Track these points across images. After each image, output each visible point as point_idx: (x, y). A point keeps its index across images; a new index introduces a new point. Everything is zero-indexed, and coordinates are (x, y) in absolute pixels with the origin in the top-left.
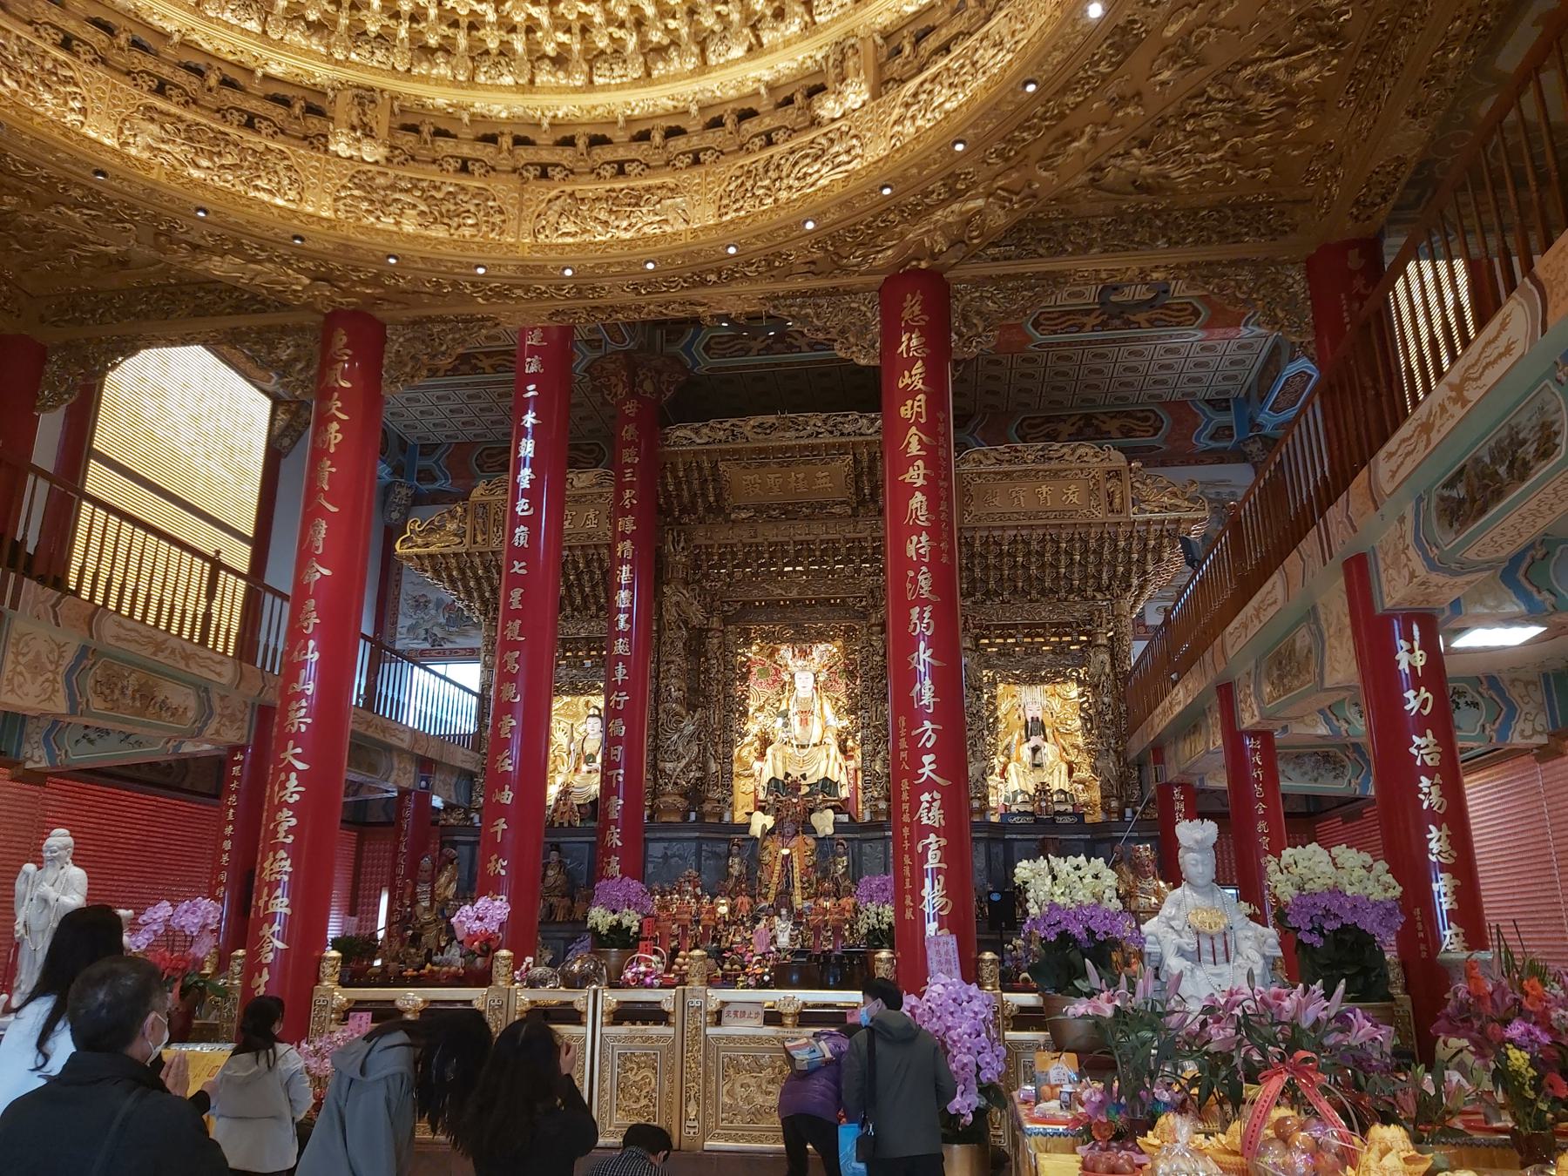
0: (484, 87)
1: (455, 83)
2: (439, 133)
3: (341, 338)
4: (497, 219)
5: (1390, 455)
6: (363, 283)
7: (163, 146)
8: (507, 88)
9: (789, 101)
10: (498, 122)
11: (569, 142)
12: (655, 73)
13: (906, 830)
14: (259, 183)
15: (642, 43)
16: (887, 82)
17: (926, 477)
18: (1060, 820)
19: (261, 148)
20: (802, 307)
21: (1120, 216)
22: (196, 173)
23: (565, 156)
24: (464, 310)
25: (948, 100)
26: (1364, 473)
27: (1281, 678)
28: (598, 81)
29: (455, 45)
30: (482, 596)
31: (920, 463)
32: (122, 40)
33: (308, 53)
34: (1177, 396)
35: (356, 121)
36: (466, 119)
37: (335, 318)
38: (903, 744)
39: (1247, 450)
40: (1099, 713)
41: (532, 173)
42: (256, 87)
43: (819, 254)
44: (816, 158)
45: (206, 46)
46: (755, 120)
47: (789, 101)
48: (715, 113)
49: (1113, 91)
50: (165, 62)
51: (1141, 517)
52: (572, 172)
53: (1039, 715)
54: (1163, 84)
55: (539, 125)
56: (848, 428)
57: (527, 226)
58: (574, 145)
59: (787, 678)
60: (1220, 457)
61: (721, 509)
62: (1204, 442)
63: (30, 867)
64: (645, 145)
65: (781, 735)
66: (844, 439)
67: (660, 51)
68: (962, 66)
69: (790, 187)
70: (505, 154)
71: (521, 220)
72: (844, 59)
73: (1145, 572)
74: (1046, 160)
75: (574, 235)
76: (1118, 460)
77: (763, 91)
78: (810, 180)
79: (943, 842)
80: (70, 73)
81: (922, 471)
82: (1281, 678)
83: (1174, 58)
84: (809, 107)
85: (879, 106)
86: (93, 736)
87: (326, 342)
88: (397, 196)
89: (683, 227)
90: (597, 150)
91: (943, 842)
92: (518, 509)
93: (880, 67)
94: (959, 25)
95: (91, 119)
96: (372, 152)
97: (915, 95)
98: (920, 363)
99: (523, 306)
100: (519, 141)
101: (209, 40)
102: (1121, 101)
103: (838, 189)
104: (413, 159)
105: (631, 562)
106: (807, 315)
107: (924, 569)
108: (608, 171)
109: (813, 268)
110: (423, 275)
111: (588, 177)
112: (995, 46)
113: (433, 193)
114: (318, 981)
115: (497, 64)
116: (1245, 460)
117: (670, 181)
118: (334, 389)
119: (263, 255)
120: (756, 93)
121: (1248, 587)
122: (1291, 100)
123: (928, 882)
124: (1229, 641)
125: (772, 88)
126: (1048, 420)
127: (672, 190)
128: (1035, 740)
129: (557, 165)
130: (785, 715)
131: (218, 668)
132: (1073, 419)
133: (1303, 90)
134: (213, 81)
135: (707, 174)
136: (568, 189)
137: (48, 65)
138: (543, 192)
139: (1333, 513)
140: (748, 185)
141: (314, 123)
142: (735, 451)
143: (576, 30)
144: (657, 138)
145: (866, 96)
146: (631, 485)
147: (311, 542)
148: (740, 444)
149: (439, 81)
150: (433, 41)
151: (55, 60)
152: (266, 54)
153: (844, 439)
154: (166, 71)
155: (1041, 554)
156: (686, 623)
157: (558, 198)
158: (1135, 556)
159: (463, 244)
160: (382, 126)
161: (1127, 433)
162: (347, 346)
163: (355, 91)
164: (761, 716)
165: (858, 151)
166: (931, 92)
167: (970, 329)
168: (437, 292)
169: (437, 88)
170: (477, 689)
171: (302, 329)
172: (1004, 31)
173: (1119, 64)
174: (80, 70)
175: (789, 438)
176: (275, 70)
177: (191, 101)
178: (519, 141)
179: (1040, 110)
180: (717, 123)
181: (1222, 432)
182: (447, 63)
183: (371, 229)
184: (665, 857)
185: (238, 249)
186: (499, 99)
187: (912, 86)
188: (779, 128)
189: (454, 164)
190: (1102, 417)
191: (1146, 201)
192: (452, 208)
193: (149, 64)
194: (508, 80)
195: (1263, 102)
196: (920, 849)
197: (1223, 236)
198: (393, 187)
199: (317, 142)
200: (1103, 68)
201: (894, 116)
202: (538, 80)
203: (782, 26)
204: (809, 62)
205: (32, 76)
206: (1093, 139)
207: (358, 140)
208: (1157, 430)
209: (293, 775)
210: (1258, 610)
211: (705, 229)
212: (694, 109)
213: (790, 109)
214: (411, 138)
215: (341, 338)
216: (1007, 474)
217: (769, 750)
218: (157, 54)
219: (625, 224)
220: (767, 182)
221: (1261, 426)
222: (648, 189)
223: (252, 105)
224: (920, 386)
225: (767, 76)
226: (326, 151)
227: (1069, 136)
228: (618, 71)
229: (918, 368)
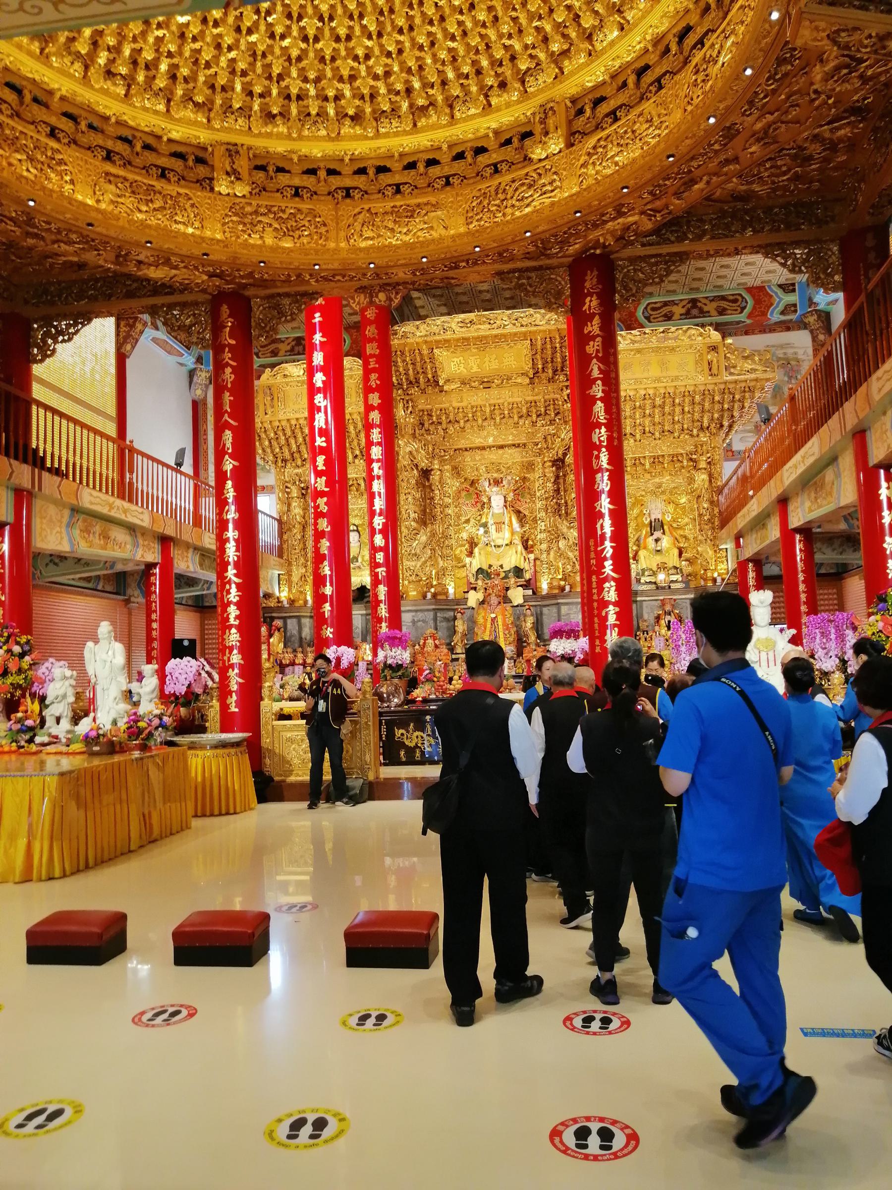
0: (308, 138)
1: (289, 137)
2: (280, 170)
3: (225, 310)
4: (323, 230)
5: (879, 379)
6: (242, 277)
7: (119, 200)
8: (322, 138)
9: (508, 142)
10: (316, 160)
11: (362, 171)
12: (419, 124)
13: (595, 604)
14: (177, 218)
15: (411, 106)
16: (575, 133)
17: (603, 391)
18: (673, 586)
19: (174, 194)
20: (519, 278)
21: (723, 214)
22: (141, 216)
23: (360, 181)
24: (302, 289)
25: (617, 155)
26: (865, 385)
27: (816, 498)
28: (382, 130)
29: (289, 113)
30: (272, 452)
31: (599, 382)
32: (83, 126)
33: (195, 123)
34: (758, 283)
35: (229, 169)
36: (296, 160)
37: (218, 299)
38: (592, 555)
39: (806, 321)
40: (700, 515)
41: (340, 194)
42: (164, 148)
43: (534, 249)
44: (530, 186)
45: (131, 123)
46: (486, 155)
47: (508, 142)
48: (459, 149)
49: (722, 157)
50: (108, 137)
51: (730, 378)
52: (366, 193)
53: (660, 517)
54: (751, 153)
55: (342, 160)
56: (525, 321)
57: (342, 234)
58: (367, 174)
59: (485, 500)
60: (787, 327)
61: (437, 383)
62: (775, 316)
63: (90, 644)
64: (413, 172)
65: (484, 539)
66: (523, 329)
67: (423, 109)
68: (626, 132)
69: (513, 206)
70: (322, 183)
71: (338, 229)
72: (546, 117)
73: (732, 416)
74: (678, 194)
75: (372, 239)
76: (716, 336)
77: (491, 135)
78: (526, 202)
79: (617, 609)
80: (61, 157)
81: (601, 388)
82: (816, 498)
83: (758, 140)
84: (522, 148)
85: (571, 153)
86: (57, 561)
87: (215, 315)
88: (260, 218)
89: (443, 232)
90: (382, 176)
91: (617, 609)
92: (316, 401)
93: (570, 122)
94: (622, 98)
95: (78, 187)
96: (241, 190)
97: (594, 148)
98: (597, 317)
99: (339, 284)
100: (331, 172)
101: (134, 118)
102: (727, 162)
103: (547, 212)
104: (265, 190)
105: (379, 426)
106: (523, 284)
107: (604, 450)
108: (389, 192)
109: (528, 256)
110: (280, 272)
111: (376, 196)
112: (647, 121)
113: (281, 214)
114: (262, 699)
115: (315, 122)
116: (805, 328)
117: (433, 200)
118: (225, 346)
119: (182, 265)
120: (487, 136)
121: (800, 441)
122: (833, 147)
123: (608, 632)
124: (786, 475)
125: (497, 133)
126: (666, 304)
127: (433, 205)
128: (657, 534)
129: (356, 188)
130: (485, 525)
131: (141, 517)
132: (684, 303)
133: (840, 140)
134: (138, 148)
135: (457, 195)
136: (367, 207)
137: (49, 154)
138: (348, 208)
139: (847, 405)
140: (485, 203)
141: (202, 171)
142: (446, 341)
143: (367, 98)
144: (421, 167)
145: (562, 146)
146: (374, 370)
147: (224, 445)
148: (449, 335)
149: (279, 136)
150: (275, 111)
151: (52, 149)
152: (169, 126)
153: (523, 329)
154: (110, 144)
155: (662, 406)
156: (417, 466)
157: (360, 213)
158: (726, 406)
159: (303, 250)
160: (244, 170)
161: (722, 312)
162: (229, 316)
163: (225, 147)
164: (468, 527)
165: (558, 183)
166: (605, 147)
167: (627, 291)
168: (287, 281)
169: (276, 141)
170: (276, 515)
171: (196, 304)
172: (654, 113)
173: (725, 145)
174: (70, 154)
175: (484, 330)
176: (175, 135)
177: (127, 163)
178: (331, 172)
179: (676, 170)
180: (460, 156)
181: (790, 308)
182: (284, 124)
183: (245, 245)
184: (414, 622)
185: (167, 262)
186: (317, 147)
187: (592, 141)
188: (503, 161)
189: (290, 192)
190: (704, 301)
191: (739, 205)
192: (294, 224)
193: (99, 140)
194: (323, 132)
195: (815, 149)
196: (604, 614)
197: (788, 227)
198: (256, 212)
199: (207, 184)
200: (716, 147)
201: (581, 161)
202: (342, 132)
203: (505, 96)
204: (522, 117)
205: (42, 163)
206: (708, 183)
207: (232, 182)
208: (743, 309)
209: (233, 586)
210: (803, 457)
211: (460, 235)
212: (445, 147)
213: (509, 148)
214: (261, 174)
215: (225, 310)
216: (639, 351)
217: (476, 550)
218: (102, 132)
219: (405, 230)
220: (497, 202)
221: (816, 304)
222: (418, 205)
223: (164, 162)
224: (598, 332)
225: (494, 125)
226: (212, 189)
227: (693, 182)
228: (395, 123)
229: (596, 320)
